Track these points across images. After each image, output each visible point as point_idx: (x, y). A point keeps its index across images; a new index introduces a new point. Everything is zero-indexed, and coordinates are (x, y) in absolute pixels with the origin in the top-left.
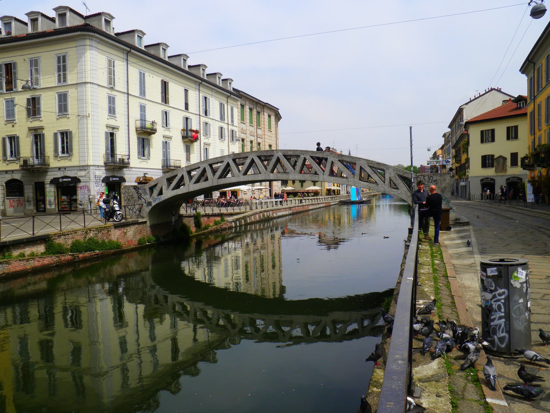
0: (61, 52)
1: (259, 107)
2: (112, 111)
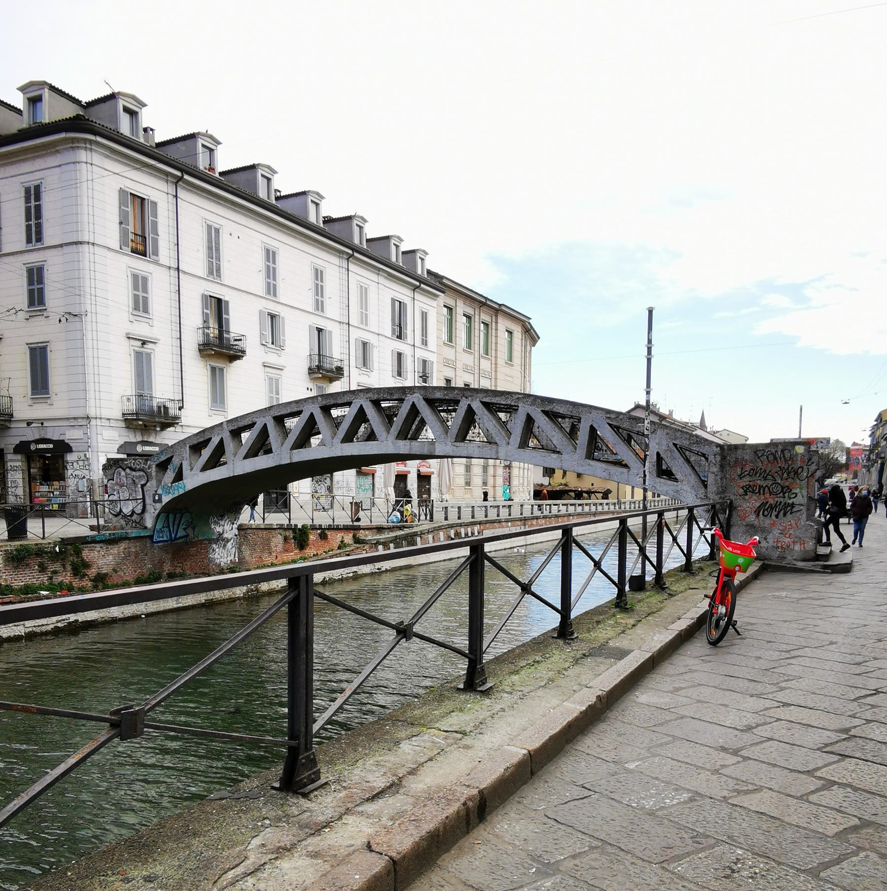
0: (31, 180)
1: (485, 313)
2: (141, 305)
